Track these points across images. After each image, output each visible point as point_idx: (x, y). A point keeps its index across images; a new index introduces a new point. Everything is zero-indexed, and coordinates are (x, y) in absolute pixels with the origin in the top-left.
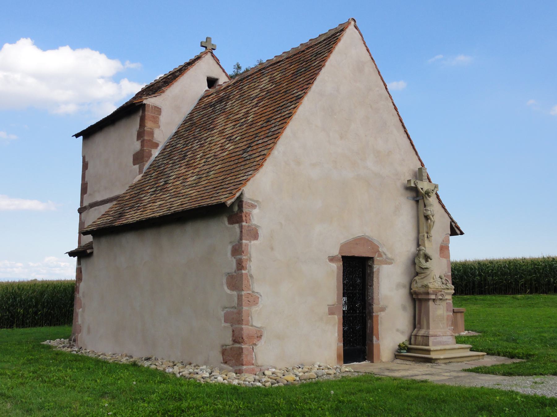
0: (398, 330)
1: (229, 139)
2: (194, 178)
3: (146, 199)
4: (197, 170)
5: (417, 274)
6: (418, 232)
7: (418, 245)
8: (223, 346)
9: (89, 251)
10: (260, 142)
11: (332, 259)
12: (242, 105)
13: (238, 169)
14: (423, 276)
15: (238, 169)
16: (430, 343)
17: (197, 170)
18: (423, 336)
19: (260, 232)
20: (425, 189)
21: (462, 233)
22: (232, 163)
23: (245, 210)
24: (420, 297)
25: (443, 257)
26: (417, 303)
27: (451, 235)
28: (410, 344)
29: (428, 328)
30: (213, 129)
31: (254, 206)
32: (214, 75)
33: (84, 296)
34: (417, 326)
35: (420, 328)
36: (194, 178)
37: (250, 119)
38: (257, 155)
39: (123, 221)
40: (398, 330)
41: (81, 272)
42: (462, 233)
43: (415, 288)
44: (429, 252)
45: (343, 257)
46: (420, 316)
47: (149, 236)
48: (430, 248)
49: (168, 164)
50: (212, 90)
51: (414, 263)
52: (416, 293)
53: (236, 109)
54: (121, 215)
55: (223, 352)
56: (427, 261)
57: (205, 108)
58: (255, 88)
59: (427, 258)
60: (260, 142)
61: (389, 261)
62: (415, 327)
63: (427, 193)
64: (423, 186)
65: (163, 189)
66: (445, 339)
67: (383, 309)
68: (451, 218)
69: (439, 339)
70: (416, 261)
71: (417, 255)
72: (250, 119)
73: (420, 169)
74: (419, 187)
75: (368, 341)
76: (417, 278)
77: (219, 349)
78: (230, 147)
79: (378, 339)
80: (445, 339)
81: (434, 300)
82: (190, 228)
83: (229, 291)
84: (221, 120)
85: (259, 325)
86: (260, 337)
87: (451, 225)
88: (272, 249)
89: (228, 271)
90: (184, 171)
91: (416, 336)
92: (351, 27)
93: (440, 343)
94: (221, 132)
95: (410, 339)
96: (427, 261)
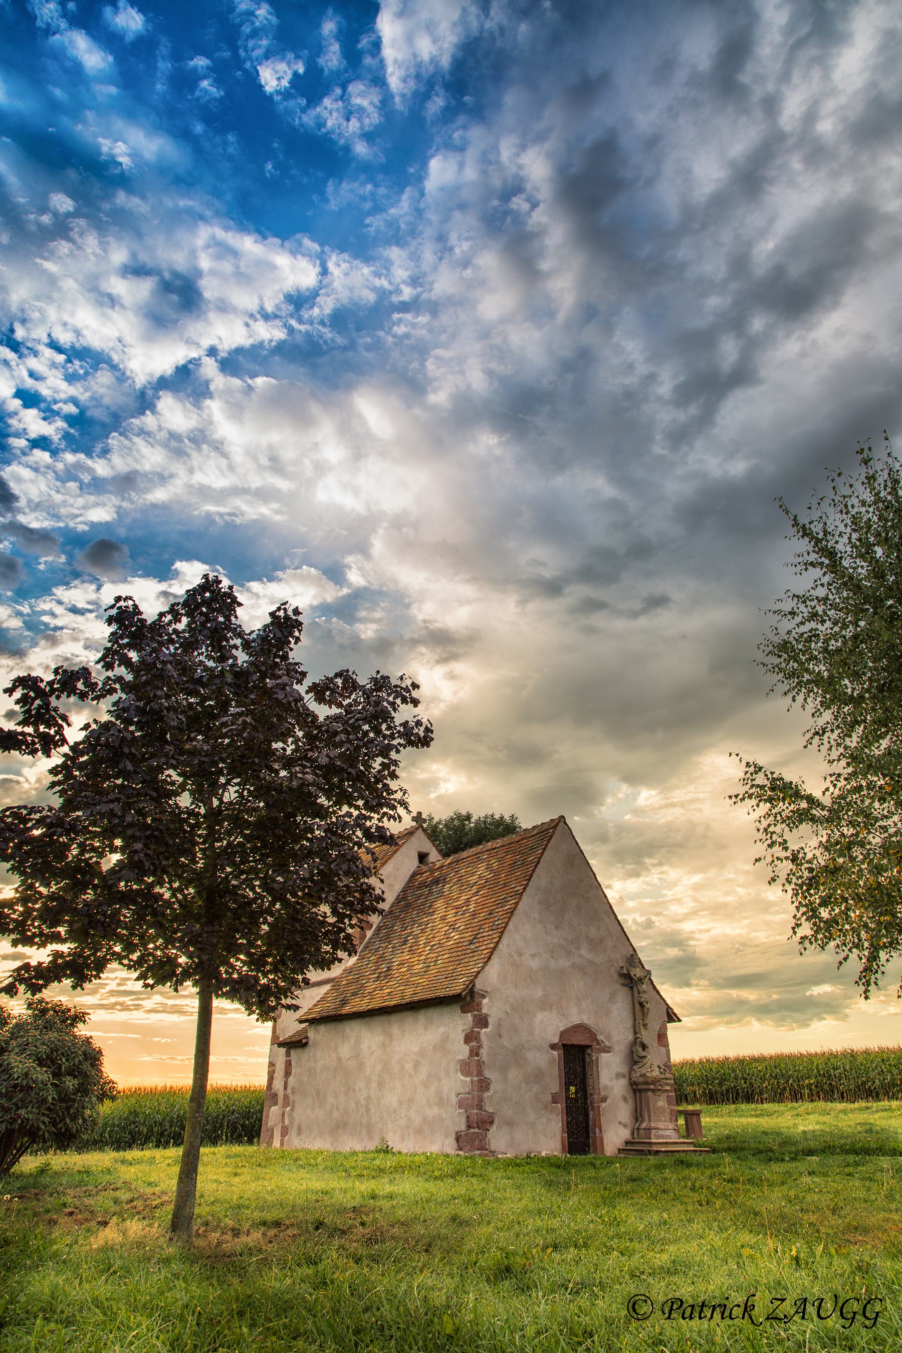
0: (620, 1123)
1: (454, 928)
2: (420, 966)
3: (371, 986)
4: (423, 957)
5: (636, 1063)
6: (635, 1020)
7: (635, 1033)
8: (457, 1133)
9: (304, 1041)
10: (485, 934)
11: (553, 1047)
12: (461, 892)
13: (466, 960)
14: (641, 1065)
15: (466, 960)
16: (652, 1136)
17: (423, 957)
18: (645, 1129)
19: (490, 1020)
20: (638, 975)
21: (679, 1020)
22: (460, 953)
23: (476, 1000)
24: (639, 1087)
25: (662, 1046)
26: (638, 1093)
27: (669, 1022)
28: (633, 1138)
29: (650, 1120)
30: (432, 914)
31: (484, 997)
32: (424, 850)
33: (293, 1092)
34: (640, 1119)
35: (642, 1121)
36: (420, 966)
37: (472, 907)
38: (483, 947)
39: (347, 1009)
40: (620, 1123)
41: (290, 1064)
42: (679, 1020)
43: (635, 1076)
44: (646, 1041)
45: (563, 1045)
46: (641, 1107)
47: (378, 1023)
48: (648, 1037)
49: (386, 947)
50: (424, 868)
51: (632, 1053)
52: (636, 1083)
53: (455, 895)
54: (344, 1002)
55: (458, 1139)
56: (644, 1050)
57: (419, 888)
58: (473, 874)
59: (644, 1047)
60: (485, 934)
61: (607, 1050)
62: (637, 1120)
63: (641, 980)
64: (637, 973)
65: (387, 974)
66: (667, 1133)
67: (604, 1100)
68: (667, 1004)
69: (661, 1132)
70: (634, 1050)
71: (634, 1043)
72: (472, 907)
73: (632, 955)
74: (632, 974)
75: (591, 1135)
76: (635, 1067)
77: (454, 1136)
78: (455, 935)
79: (601, 1131)
80: (667, 1133)
81: (653, 1090)
82: (422, 1016)
83: (462, 1078)
84: (439, 904)
85: (491, 1111)
86: (492, 1123)
87: (668, 1012)
88: (500, 1036)
89: (461, 1057)
90: (408, 957)
91: (638, 1129)
92: (561, 824)
93: (662, 1137)
94: (443, 918)
95: (633, 1134)
96: (644, 1050)
